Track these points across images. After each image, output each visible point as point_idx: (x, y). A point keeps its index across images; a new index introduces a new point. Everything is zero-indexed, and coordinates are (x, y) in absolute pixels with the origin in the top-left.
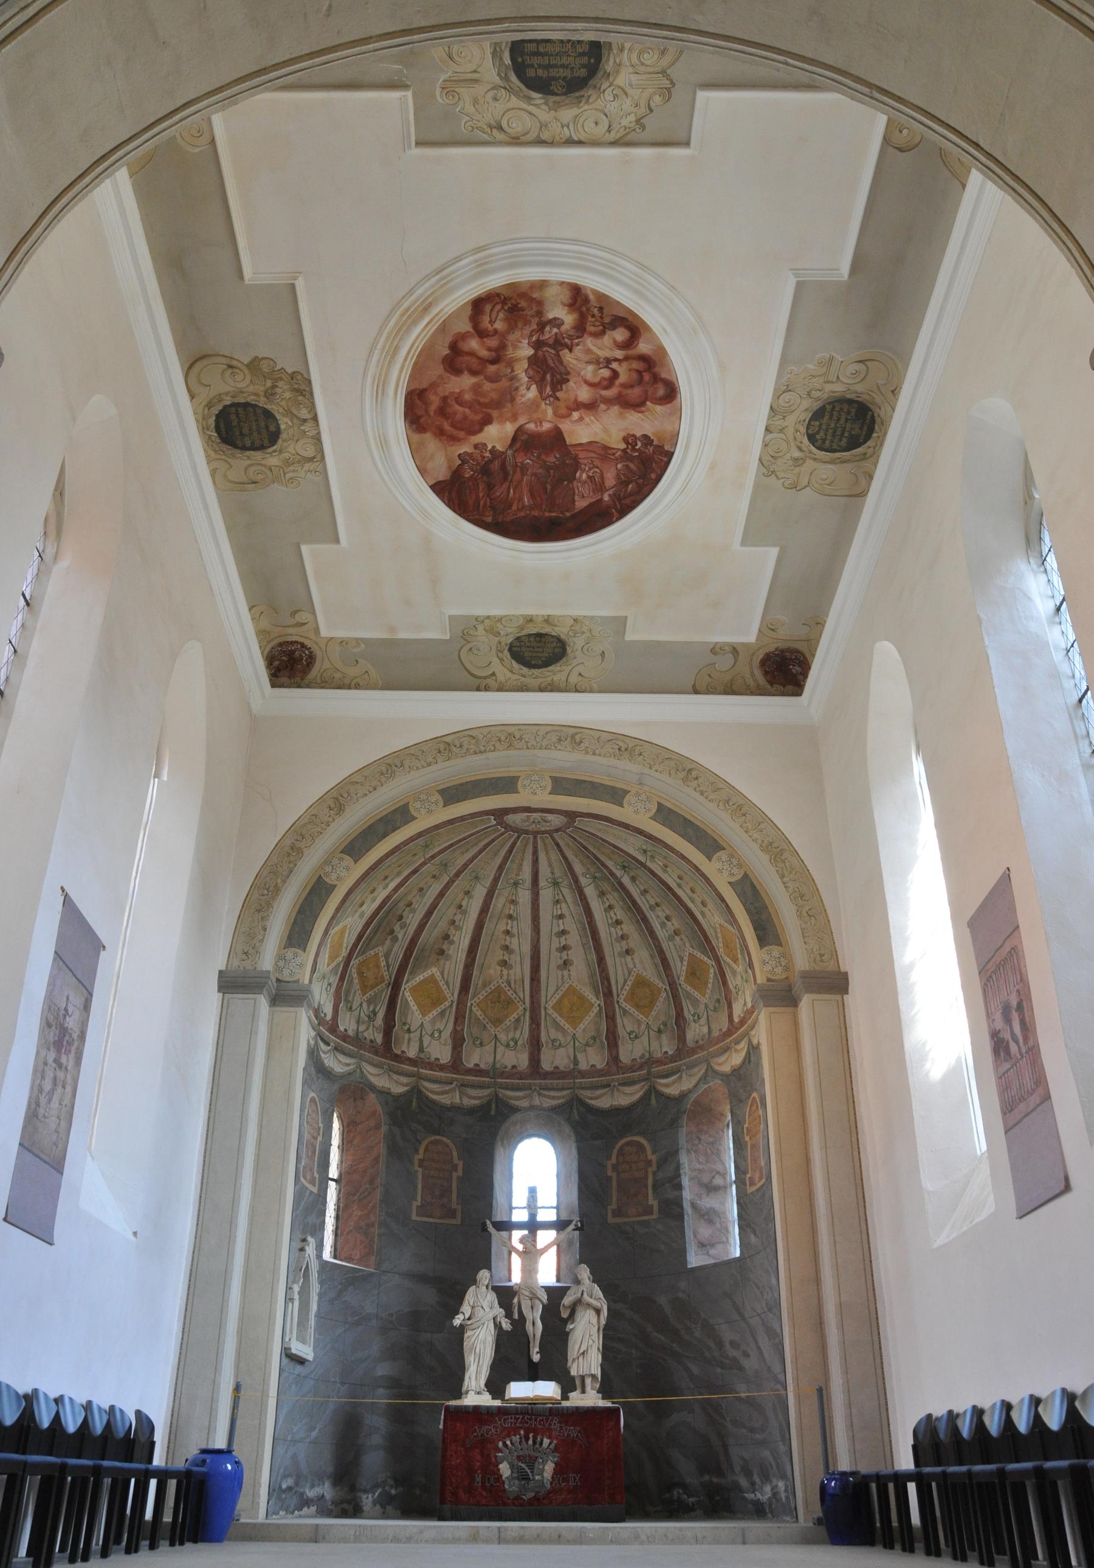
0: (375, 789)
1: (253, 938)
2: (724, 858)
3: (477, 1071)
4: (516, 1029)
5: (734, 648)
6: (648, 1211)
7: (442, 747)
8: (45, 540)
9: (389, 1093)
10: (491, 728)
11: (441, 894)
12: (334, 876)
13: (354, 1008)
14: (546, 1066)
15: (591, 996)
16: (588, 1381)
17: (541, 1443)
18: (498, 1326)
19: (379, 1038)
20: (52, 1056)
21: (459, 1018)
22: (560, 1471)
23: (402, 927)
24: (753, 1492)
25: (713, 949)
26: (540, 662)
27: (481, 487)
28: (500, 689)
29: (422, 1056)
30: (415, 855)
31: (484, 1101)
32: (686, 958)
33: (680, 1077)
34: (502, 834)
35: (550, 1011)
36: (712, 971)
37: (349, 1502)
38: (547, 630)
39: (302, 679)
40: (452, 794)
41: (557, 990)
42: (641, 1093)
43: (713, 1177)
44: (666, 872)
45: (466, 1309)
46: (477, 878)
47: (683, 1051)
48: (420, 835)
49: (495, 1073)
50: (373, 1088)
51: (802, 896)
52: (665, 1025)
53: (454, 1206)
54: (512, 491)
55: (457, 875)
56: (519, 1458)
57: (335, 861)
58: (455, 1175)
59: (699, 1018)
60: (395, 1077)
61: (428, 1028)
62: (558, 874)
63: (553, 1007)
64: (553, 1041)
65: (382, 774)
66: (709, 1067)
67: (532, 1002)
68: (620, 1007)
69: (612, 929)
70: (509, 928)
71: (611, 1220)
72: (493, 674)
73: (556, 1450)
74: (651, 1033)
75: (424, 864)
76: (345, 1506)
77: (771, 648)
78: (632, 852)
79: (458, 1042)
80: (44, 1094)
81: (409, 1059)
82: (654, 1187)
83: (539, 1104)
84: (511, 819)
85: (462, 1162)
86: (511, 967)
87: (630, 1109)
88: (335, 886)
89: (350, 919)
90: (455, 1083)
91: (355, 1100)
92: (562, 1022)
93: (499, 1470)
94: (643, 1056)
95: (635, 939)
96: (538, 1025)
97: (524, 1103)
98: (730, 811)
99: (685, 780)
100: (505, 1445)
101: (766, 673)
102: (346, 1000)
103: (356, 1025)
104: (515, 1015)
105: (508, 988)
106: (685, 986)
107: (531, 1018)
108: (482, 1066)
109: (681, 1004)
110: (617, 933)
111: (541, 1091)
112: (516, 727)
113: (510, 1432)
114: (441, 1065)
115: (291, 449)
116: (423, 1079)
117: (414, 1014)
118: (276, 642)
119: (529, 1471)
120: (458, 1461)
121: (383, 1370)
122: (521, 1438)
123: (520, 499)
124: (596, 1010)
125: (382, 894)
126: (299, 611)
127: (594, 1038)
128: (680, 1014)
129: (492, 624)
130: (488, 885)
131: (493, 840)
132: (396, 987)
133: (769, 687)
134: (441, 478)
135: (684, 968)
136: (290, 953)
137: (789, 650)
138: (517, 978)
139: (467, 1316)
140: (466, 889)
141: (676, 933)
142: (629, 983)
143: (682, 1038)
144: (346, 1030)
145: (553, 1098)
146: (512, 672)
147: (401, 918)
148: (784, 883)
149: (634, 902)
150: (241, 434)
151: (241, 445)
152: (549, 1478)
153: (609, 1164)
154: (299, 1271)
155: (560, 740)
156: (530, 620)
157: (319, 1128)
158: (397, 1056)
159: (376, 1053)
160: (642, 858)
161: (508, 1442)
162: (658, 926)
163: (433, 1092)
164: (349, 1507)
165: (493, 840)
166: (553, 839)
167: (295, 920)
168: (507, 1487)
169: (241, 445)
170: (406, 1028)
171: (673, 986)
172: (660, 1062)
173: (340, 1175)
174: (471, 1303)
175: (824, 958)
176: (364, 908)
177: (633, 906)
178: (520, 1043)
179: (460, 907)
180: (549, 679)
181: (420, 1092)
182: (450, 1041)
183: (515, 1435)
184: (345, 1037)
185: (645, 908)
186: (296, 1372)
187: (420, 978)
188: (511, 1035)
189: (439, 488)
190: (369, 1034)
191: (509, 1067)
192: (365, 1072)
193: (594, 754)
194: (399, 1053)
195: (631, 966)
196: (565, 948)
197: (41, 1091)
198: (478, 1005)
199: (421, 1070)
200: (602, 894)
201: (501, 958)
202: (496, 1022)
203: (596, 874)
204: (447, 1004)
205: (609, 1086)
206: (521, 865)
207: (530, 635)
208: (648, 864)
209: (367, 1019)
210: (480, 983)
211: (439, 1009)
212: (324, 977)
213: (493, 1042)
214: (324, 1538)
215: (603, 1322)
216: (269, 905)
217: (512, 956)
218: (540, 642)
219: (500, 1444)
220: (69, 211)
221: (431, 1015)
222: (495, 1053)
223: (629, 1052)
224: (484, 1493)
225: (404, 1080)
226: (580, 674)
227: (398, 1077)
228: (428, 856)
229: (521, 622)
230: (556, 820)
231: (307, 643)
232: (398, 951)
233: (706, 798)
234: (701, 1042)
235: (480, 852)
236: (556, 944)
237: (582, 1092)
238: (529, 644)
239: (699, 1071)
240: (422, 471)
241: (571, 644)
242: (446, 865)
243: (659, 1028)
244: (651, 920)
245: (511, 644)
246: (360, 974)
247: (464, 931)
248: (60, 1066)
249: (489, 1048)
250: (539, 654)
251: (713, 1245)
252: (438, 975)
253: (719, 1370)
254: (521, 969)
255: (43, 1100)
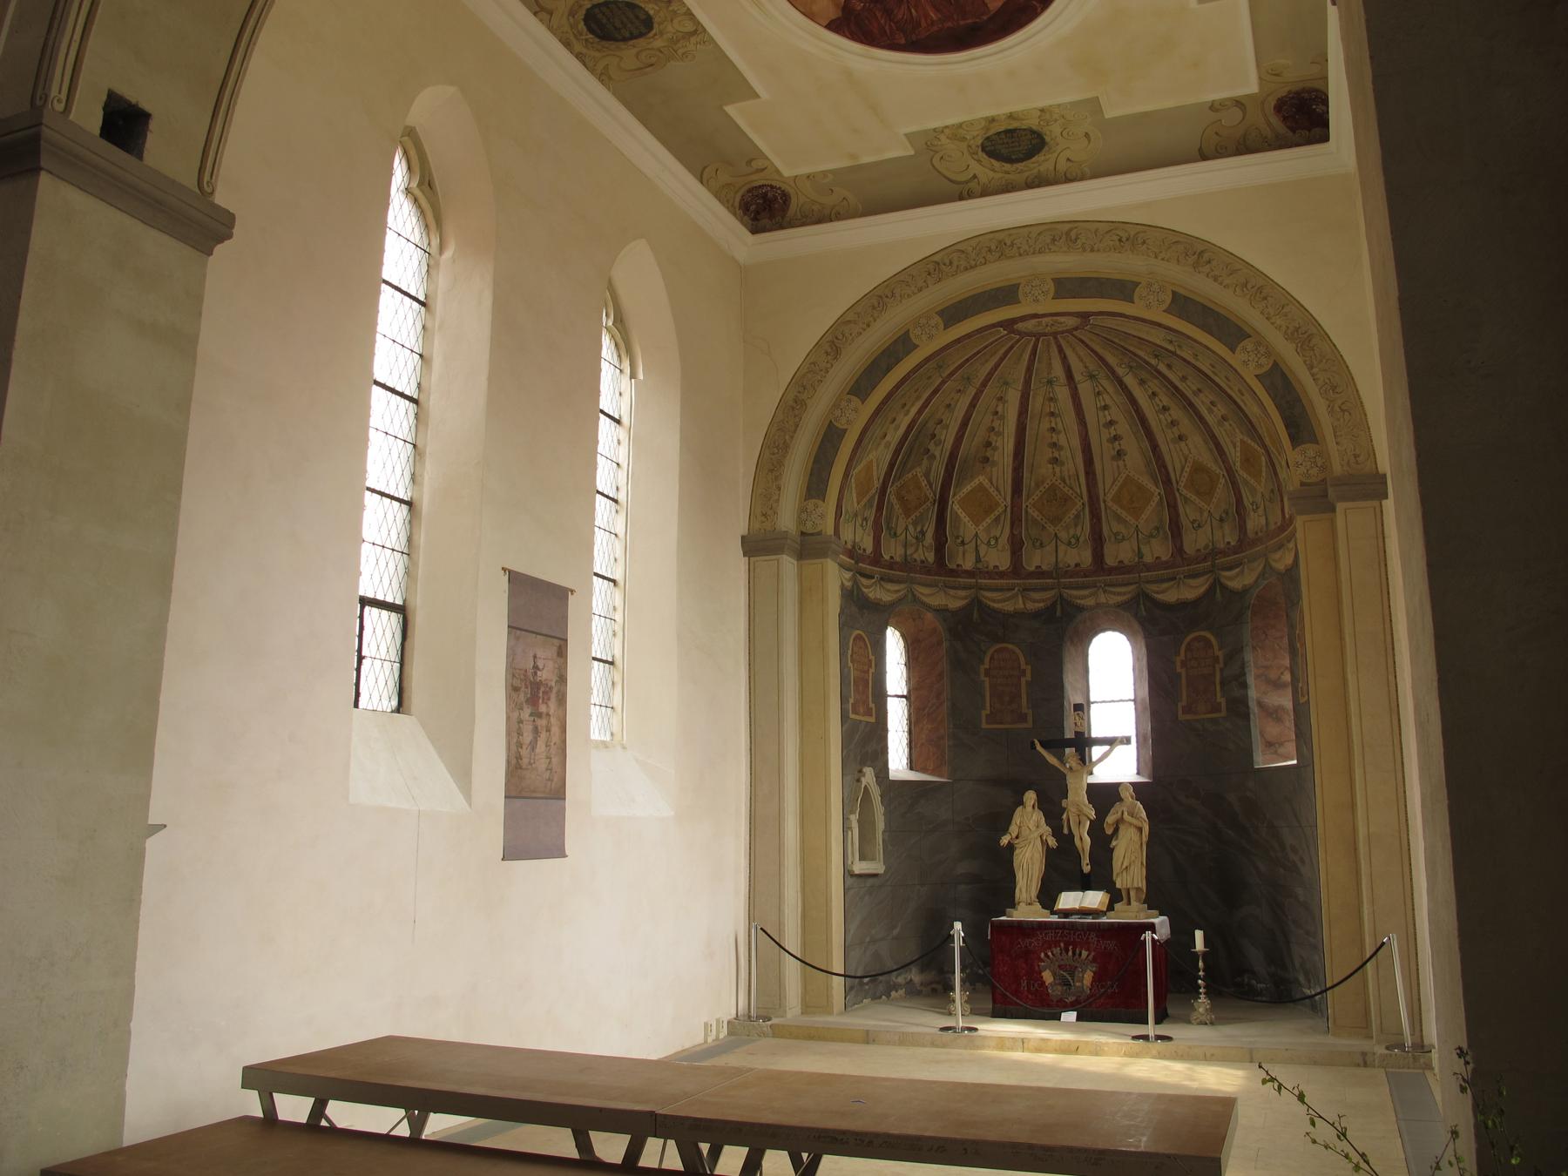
0: (868, 326)
1: (769, 500)
2: (1250, 347)
3: (1040, 573)
4: (1076, 526)
5: (1237, 101)
6: (1216, 708)
7: (931, 267)
8: (428, 235)
9: (947, 610)
10: (980, 238)
11: (973, 405)
12: (844, 420)
13: (899, 533)
14: (1110, 561)
15: (1151, 486)
16: (1132, 894)
17: (1080, 955)
18: (1044, 843)
19: (931, 557)
20: (526, 713)
21: (1015, 521)
22: (1098, 978)
23: (936, 445)
24: (1309, 989)
25: (1261, 438)
26: (1021, 156)
27: (879, 15)
28: (985, 193)
29: (979, 566)
30: (930, 378)
31: (1049, 603)
32: (1238, 444)
33: (1242, 571)
34: (1018, 341)
35: (1110, 504)
36: (1263, 458)
37: (938, 983)
38: (1014, 125)
39: (783, 218)
40: (953, 313)
41: (1114, 481)
42: (1206, 586)
43: (1282, 673)
44: (1197, 360)
45: (1013, 829)
46: (1006, 383)
47: (1243, 543)
48: (928, 360)
49: (1058, 572)
50: (928, 607)
51: (1334, 388)
52: (1227, 513)
53: (1024, 710)
54: (913, 11)
55: (984, 384)
56: (1060, 966)
57: (844, 404)
58: (1023, 680)
59: (1257, 508)
60: (952, 592)
61: (983, 536)
62: (1091, 367)
63: (1112, 500)
64: (1116, 534)
65: (874, 308)
66: (1267, 565)
67: (1090, 497)
68: (1181, 495)
69: (1161, 416)
70: (1053, 425)
71: (1181, 717)
72: (975, 177)
73: (1094, 960)
74: (1213, 520)
75: (943, 382)
76: (934, 986)
77: (1283, 92)
78: (1158, 342)
79: (1016, 546)
80: (524, 747)
81: (966, 572)
82: (1222, 683)
83: (1105, 601)
84: (1020, 326)
85: (1029, 667)
86: (1062, 464)
87: (1195, 603)
88: (845, 431)
89: (874, 453)
90: (1016, 589)
91: (914, 620)
92: (1124, 514)
93: (1042, 977)
94: (1206, 547)
95: (1186, 425)
96: (1099, 520)
97: (1090, 602)
98: (1248, 296)
99: (1196, 266)
100: (1046, 955)
101: (1285, 119)
102: (889, 528)
103: (903, 550)
104: (1074, 511)
105: (1063, 484)
106: (1241, 472)
107: (1091, 512)
108: (1044, 568)
109: (1240, 492)
110: (1166, 420)
111: (1106, 588)
112: (1007, 232)
113: (1050, 945)
114: (1001, 572)
115: (670, 28)
116: (981, 589)
117: (965, 524)
118: (745, 188)
119: (1070, 978)
120: (1005, 969)
121: (963, 868)
122: (1061, 950)
123: (926, 16)
124: (1156, 499)
125: (905, 422)
126: (754, 159)
127: (1157, 529)
128: (1239, 501)
129: (956, 133)
130: (1020, 388)
131: (1011, 348)
132: (943, 502)
133: (1290, 134)
134: (833, 17)
135: (1238, 454)
136: (811, 504)
137: (1304, 90)
138: (1071, 473)
139: (1014, 835)
140: (998, 395)
141: (1224, 418)
142: (1186, 469)
143: (1242, 527)
144: (892, 558)
145: (1119, 594)
146: (993, 170)
147: (933, 436)
148: (1313, 375)
149: (1176, 388)
150: (616, 28)
151: (620, 37)
152: (1089, 985)
153: (1178, 660)
154: (856, 800)
155: (1054, 240)
156: (992, 120)
157: (870, 661)
158: (952, 571)
159: (929, 572)
160: (1170, 347)
161: (1050, 954)
162: (1206, 411)
163: (994, 601)
164: (939, 987)
165: (1011, 348)
166: (1076, 337)
167: (812, 470)
168: (1050, 991)
169: (620, 37)
170: (959, 541)
171: (1230, 471)
172: (1223, 553)
173: (909, 692)
174: (1018, 823)
175: (1361, 459)
176: (887, 438)
177: (1175, 391)
178: (1081, 540)
179: (997, 413)
180: (1035, 171)
181: (980, 602)
182: (1007, 547)
183: (1056, 947)
184: (891, 565)
185: (1189, 394)
186: (868, 885)
187: (968, 488)
188: (1072, 532)
189: (834, 26)
190: (919, 556)
191: (1073, 565)
192: (918, 594)
193: (1092, 250)
194: (955, 567)
195: (1186, 452)
196: (1116, 438)
197: (520, 745)
198: (1034, 505)
199: (980, 581)
200: (1142, 382)
201: (1051, 455)
202: (1056, 520)
203: (1131, 364)
204: (1000, 509)
205: (1175, 578)
206: (1050, 364)
207: (999, 134)
208: (1178, 352)
209: (914, 541)
210: (1033, 484)
211: (993, 516)
212: (856, 515)
213: (1054, 541)
214: (874, 1041)
215: (1145, 839)
216: (780, 463)
217: (1062, 453)
218: (1012, 137)
219: (1042, 955)
220: (266, 17)
221: (985, 524)
222: (1057, 551)
223: (1194, 542)
224: (1030, 996)
225: (963, 593)
226: (1068, 159)
227: (955, 591)
228: (945, 375)
229: (983, 123)
230: (1071, 322)
231: (774, 183)
232: (939, 469)
233: (1221, 284)
234: (1260, 534)
235: (1002, 359)
236: (1105, 436)
237: (1148, 586)
238: (1001, 142)
239: (1258, 566)
240: (810, 16)
241: (1048, 133)
242: (968, 378)
243: (1221, 517)
244: (1198, 407)
245: (982, 144)
246: (901, 499)
247: (1006, 435)
248: (540, 715)
249: (1050, 548)
250: (1016, 149)
251: (1281, 744)
252: (986, 483)
253: (1282, 871)
254: (1073, 463)
255: (524, 752)
